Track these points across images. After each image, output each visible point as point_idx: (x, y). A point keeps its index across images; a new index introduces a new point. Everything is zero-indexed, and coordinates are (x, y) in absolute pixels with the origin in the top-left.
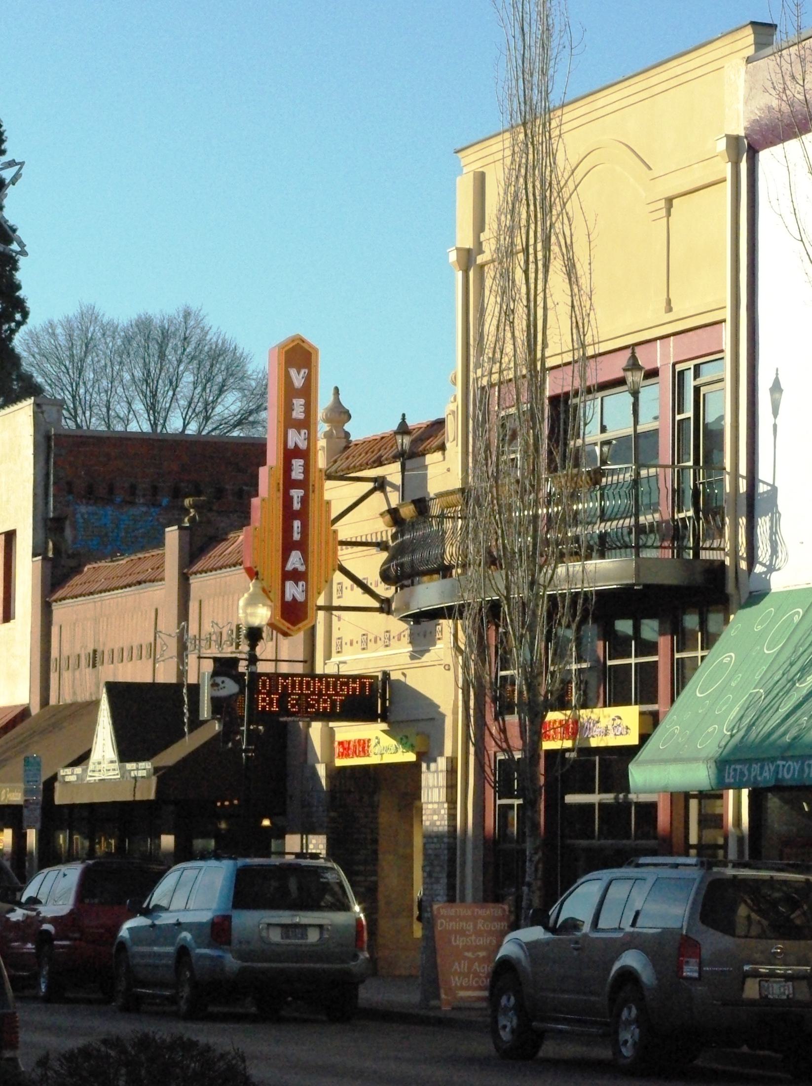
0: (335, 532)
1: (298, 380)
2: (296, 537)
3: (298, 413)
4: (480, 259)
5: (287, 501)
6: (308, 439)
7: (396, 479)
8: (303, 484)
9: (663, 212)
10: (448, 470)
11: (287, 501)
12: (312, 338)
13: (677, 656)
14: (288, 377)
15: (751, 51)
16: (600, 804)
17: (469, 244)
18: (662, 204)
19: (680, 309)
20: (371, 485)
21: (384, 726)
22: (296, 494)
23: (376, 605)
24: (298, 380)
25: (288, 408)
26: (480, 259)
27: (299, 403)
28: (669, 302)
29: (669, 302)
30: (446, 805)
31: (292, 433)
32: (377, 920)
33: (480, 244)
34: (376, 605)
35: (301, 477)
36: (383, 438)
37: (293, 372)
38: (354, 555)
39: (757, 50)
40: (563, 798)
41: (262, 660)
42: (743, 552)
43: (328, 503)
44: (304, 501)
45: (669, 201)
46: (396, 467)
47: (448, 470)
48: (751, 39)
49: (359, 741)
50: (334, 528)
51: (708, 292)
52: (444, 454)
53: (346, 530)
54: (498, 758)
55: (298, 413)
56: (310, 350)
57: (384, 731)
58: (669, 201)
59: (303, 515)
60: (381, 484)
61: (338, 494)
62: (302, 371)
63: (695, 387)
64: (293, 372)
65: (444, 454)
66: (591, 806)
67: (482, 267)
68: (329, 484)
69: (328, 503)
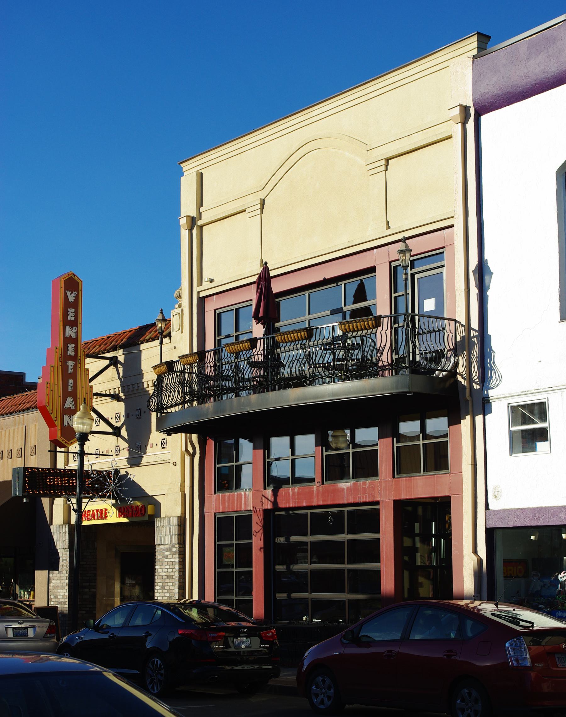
0: (91, 387)
1: (71, 299)
2: (70, 389)
3: (71, 317)
4: (200, 223)
5: (65, 367)
6: (77, 333)
7: (121, 359)
8: (74, 358)
9: (383, 168)
10: (175, 348)
11: (65, 367)
12: (80, 275)
13: (218, 466)
14: (66, 297)
15: (475, 52)
16: (377, 542)
17: (194, 214)
18: (383, 162)
19: (394, 227)
20: (107, 362)
21: (114, 501)
22: (70, 363)
23: (111, 430)
24: (71, 299)
25: (66, 314)
26: (200, 223)
27: (72, 311)
28: (388, 223)
29: (388, 223)
30: (177, 546)
31: (68, 328)
32: (95, 614)
33: (200, 213)
34: (111, 430)
35: (73, 354)
36: (108, 337)
37: (68, 293)
38: (101, 402)
39: (478, 52)
40: (274, 540)
41: (87, 454)
42: (475, 375)
43: (88, 370)
44: (75, 368)
45: (387, 160)
46: (121, 352)
47: (175, 348)
48: (475, 44)
49: (97, 511)
50: (90, 384)
51: (448, 204)
52: (170, 339)
53: (98, 386)
54: (217, 516)
55: (71, 317)
56: (78, 281)
57: (113, 505)
58: (387, 160)
59: (74, 376)
60: (114, 362)
61: (93, 365)
62: (74, 293)
63: (411, 274)
64: (68, 293)
65: (170, 339)
66: (342, 542)
67: (201, 227)
68: (88, 360)
69: (88, 370)
